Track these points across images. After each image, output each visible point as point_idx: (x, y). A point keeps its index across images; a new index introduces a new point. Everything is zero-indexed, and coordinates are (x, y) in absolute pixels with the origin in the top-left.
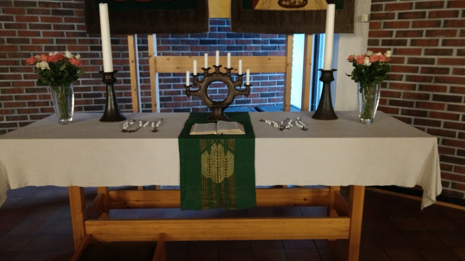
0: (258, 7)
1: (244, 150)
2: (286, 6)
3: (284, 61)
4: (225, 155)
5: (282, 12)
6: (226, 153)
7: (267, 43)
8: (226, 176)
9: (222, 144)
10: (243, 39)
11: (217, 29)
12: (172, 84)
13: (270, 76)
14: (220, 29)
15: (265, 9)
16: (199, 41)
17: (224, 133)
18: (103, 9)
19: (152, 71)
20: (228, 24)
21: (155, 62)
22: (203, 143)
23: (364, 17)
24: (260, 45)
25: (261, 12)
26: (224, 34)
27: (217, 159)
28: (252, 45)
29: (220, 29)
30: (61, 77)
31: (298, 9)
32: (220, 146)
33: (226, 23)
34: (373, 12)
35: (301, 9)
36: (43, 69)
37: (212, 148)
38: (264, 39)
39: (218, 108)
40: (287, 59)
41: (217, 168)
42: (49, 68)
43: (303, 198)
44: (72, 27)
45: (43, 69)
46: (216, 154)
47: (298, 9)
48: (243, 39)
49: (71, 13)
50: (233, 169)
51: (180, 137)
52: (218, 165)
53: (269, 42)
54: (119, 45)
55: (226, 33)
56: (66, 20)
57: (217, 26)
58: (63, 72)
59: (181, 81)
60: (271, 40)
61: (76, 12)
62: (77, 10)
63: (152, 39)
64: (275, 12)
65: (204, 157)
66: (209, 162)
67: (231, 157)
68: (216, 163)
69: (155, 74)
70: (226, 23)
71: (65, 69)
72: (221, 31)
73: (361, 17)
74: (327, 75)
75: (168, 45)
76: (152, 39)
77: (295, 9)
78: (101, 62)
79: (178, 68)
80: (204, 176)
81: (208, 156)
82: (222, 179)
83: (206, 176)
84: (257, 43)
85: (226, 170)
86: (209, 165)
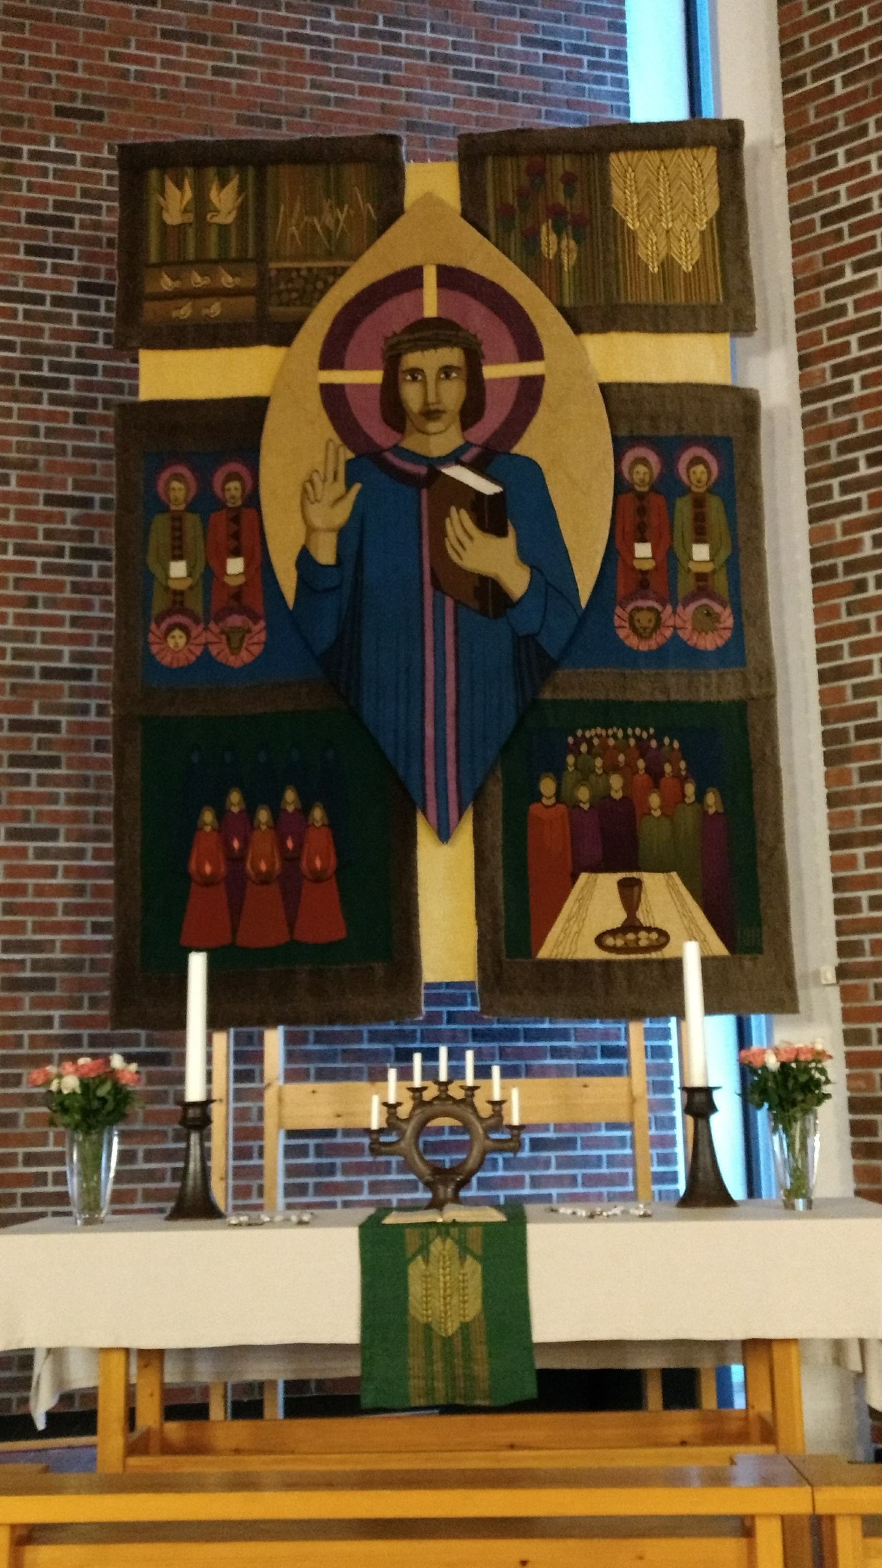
0: (545, 953)
1: (503, 1257)
2: (614, 949)
3: (625, 1089)
4: (462, 1264)
5: (608, 963)
6: (462, 1259)
7: (594, 1056)
8: (464, 1317)
9: (453, 1239)
10: (521, 1044)
11: (445, 1017)
12: (311, 1181)
13: (608, 1156)
14: (452, 1018)
15: (564, 957)
16: (393, 1050)
17: (458, 1220)
18: (197, 965)
19: (270, 1123)
20: (474, 1003)
21: (280, 1100)
22: (412, 1241)
23: (825, 972)
24: (573, 1062)
25: (554, 965)
26: (466, 1031)
27: (444, 1276)
28: (549, 1061)
29: (452, 1018)
30: (97, 1112)
31: (648, 956)
32: (449, 1241)
33: (469, 1000)
34: (844, 961)
35: (654, 955)
36: (65, 1092)
37: (433, 1249)
38: (580, 1044)
39: (445, 1184)
40: (630, 1084)
41: (445, 1298)
42: (78, 1091)
43: (677, 1440)
44: (47, 1022)
45: (65, 1092)
46: (441, 1263)
47: (648, 956)
48: (521, 1044)
49: (49, 984)
50: (479, 1301)
51: (362, 1227)
52: (445, 1290)
53: (599, 1053)
54: (168, 1069)
55: (469, 1027)
56: (36, 1004)
57: (444, 1009)
58: (103, 1100)
59: (339, 1172)
60: (603, 1048)
61: (63, 981)
62: (66, 975)
63: (274, 1041)
64: (589, 963)
65: (416, 1269)
66: (426, 1283)
67: (473, 1269)
68: (441, 1285)
69: (278, 1133)
70: (469, 1000)
71: (109, 1093)
72: (455, 1022)
73: (817, 975)
74: (699, 1098)
75: (305, 1066)
76: (274, 1041)
77: (640, 956)
78: (181, 1079)
79: (339, 1116)
80: (414, 1318)
81: (424, 1267)
82: (456, 1325)
83: (419, 1318)
84: (561, 1057)
85: (464, 1302)
86: (427, 1289)
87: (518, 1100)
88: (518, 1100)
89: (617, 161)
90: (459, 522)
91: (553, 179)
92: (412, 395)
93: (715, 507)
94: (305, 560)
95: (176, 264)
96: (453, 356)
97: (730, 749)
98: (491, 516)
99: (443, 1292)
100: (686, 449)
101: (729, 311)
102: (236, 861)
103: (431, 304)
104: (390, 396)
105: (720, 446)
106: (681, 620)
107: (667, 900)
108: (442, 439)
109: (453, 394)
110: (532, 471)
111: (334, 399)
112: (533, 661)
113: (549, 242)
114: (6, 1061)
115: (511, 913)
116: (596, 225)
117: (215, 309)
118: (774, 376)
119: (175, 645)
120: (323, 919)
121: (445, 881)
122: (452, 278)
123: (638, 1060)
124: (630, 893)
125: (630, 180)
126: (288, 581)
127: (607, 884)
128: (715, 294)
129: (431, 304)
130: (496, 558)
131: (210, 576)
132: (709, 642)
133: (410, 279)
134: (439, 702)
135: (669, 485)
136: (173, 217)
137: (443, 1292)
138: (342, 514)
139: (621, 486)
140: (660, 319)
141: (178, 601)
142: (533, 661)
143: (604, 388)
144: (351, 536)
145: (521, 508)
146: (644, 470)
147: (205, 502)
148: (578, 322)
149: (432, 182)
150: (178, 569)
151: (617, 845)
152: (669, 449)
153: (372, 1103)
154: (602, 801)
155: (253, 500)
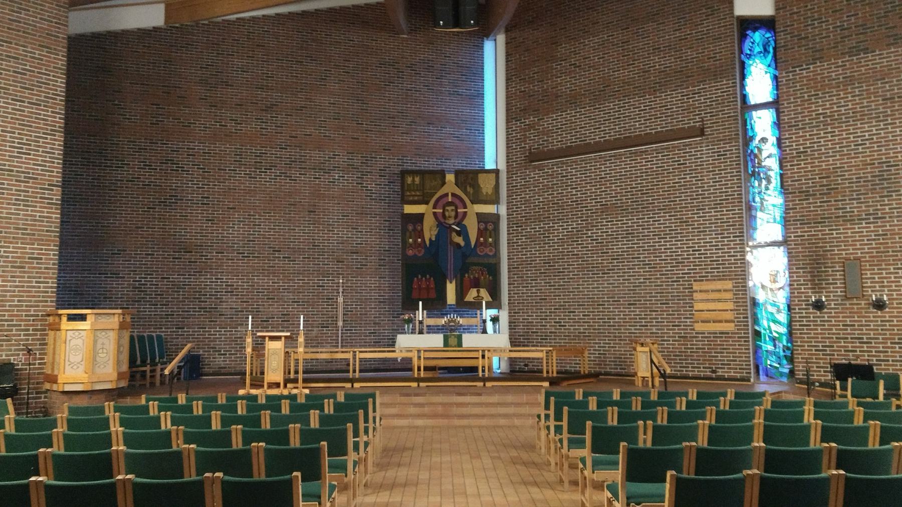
18: (421, 303)
87: (461, 321)
88: (461, 321)
89: (480, 175)
90: (454, 234)
91: (469, 178)
92: (447, 214)
93: (493, 233)
94: (430, 240)
95: (410, 190)
96: (453, 208)
97: (493, 270)
98: (459, 234)
99: (453, 341)
100: (489, 223)
101: (496, 201)
102: (419, 286)
103: (450, 199)
104: (443, 213)
105: (494, 223)
106: (487, 250)
107: (484, 293)
108: (451, 221)
109: (453, 214)
110: (465, 226)
111: (435, 214)
112: (465, 256)
113: (469, 189)
114: (2, 301)
115: (461, 293)
116: (476, 187)
117: (416, 198)
118: (503, 210)
119: (410, 252)
120: (433, 295)
121: (451, 289)
122: (453, 195)
123: (478, 315)
124: (478, 292)
125: (482, 178)
126: (428, 243)
127: (475, 290)
128: (494, 198)
129: (450, 199)
130: (459, 240)
131: (415, 241)
132: (491, 254)
133: (447, 195)
134: (450, 262)
135: (486, 229)
136: (409, 182)
137: (453, 341)
138: (436, 233)
139: (479, 229)
140: (486, 202)
141: (411, 245)
142: (465, 256)
143: (477, 214)
144: (437, 236)
145: (463, 232)
146: (482, 226)
147: (415, 230)
148: (473, 202)
149: (450, 178)
150: (411, 240)
151: (477, 284)
152: (486, 223)
153: (442, 321)
154: (475, 277)
155: (422, 230)
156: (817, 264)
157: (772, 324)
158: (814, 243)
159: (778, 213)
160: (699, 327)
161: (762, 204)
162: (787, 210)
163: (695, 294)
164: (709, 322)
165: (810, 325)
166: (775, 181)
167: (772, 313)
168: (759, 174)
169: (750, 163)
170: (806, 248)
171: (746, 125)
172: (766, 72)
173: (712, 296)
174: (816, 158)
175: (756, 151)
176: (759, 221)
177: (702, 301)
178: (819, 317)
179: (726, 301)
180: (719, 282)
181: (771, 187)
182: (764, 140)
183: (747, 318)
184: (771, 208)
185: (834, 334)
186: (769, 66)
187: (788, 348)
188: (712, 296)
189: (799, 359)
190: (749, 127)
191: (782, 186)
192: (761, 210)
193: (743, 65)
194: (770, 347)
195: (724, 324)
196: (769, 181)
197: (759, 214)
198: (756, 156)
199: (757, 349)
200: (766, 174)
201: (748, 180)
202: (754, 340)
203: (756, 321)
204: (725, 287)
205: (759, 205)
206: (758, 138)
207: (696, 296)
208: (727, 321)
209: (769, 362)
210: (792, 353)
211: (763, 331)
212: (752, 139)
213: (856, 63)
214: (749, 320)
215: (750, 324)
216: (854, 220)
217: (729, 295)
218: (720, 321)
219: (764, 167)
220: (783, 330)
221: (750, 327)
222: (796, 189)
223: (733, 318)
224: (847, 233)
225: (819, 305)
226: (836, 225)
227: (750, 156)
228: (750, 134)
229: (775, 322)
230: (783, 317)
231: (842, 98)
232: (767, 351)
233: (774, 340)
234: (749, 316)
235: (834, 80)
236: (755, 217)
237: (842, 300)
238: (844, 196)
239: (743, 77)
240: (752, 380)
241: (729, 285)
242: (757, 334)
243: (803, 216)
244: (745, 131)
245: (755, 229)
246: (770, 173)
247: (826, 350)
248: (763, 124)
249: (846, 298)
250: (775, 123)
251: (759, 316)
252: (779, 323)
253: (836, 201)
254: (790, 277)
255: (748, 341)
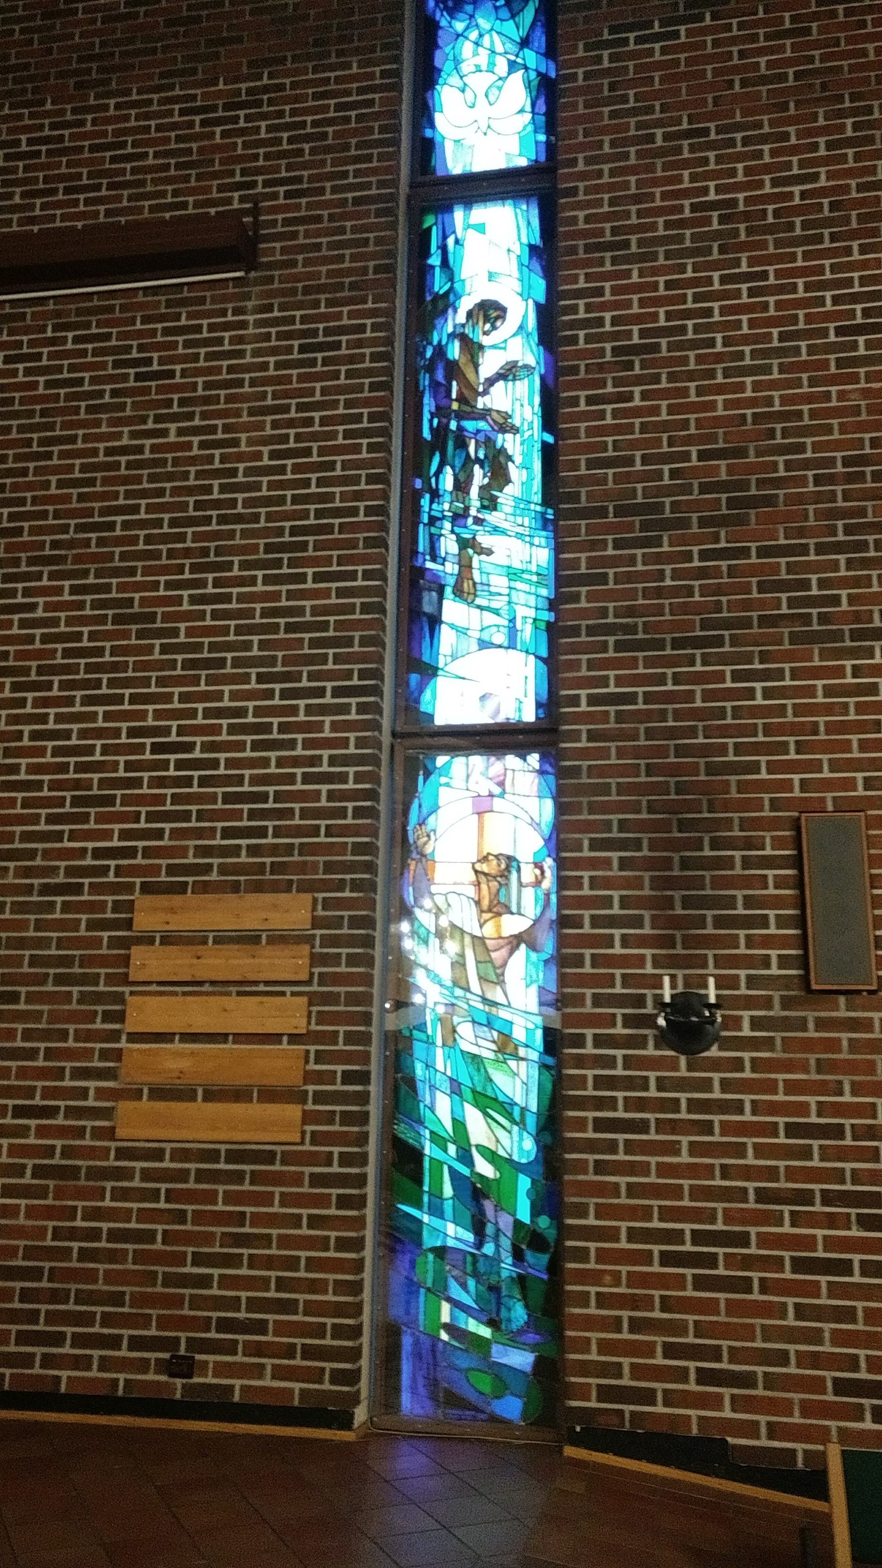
156: (683, 826)
157: (474, 1118)
158: (672, 733)
159: (529, 606)
160: (137, 1122)
161: (465, 566)
162: (565, 581)
163: (137, 953)
164: (186, 1094)
165: (642, 1127)
166: (525, 477)
167: (476, 1059)
168: (461, 443)
169: (428, 404)
170: (637, 753)
171: (425, 253)
172: (513, 66)
173: (218, 963)
174: (691, 376)
175: (454, 351)
176: (446, 637)
177: (274, 988)
178: (682, 1085)
179: (274, 988)
180: (252, 898)
181: (507, 496)
182: (490, 312)
183: (363, 1078)
184: (499, 582)
185: (747, 1173)
186: (525, 43)
187: (537, 1241)
188: (218, 963)
189: (586, 1303)
190: (435, 260)
191: (548, 499)
192: (458, 592)
193: (428, 38)
194: (455, 1234)
195: (255, 1110)
196: (499, 474)
197: (452, 610)
198: (453, 369)
199: (400, 1238)
200: (489, 442)
201: (415, 465)
202: (390, 1191)
203: (402, 1091)
204: (279, 921)
205: (451, 568)
206: (466, 304)
207: (147, 962)
208: (270, 1095)
209: (446, 1313)
210: (554, 1268)
211: (429, 1149)
212: (445, 303)
213: (844, 27)
214: (374, 1089)
215: (374, 1109)
216: (838, 636)
217: (290, 963)
218: (240, 1095)
219: (484, 414)
220: (522, 1146)
221: (373, 1128)
222: (607, 495)
223: (294, 1078)
224: (810, 691)
225: (688, 1027)
226: (764, 657)
227: (431, 368)
228: (439, 284)
229: (489, 1102)
230: (521, 1083)
231: (794, 150)
232: (441, 1252)
233: (475, 1195)
234: (375, 1068)
235: (764, 80)
236: (435, 621)
237: (787, 1003)
238: (801, 532)
239: (428, 77)
240: (361, 1414)
241: (294, 911)
242: (406, 1161)
243: (631, 612)
244: (420, 273)
245: (430, 672)
246: (508, 442)
247: (711, 1261)
248: (491, 255)
249: (807, 991)
250: (532, 248)
251: (419, 1070)
252: (506, 1108)
253: (763, 552)
254: (562, 883)
255: (360, 1202)
